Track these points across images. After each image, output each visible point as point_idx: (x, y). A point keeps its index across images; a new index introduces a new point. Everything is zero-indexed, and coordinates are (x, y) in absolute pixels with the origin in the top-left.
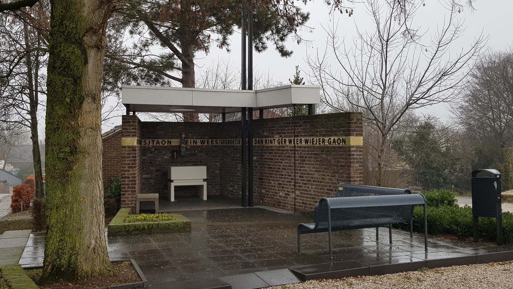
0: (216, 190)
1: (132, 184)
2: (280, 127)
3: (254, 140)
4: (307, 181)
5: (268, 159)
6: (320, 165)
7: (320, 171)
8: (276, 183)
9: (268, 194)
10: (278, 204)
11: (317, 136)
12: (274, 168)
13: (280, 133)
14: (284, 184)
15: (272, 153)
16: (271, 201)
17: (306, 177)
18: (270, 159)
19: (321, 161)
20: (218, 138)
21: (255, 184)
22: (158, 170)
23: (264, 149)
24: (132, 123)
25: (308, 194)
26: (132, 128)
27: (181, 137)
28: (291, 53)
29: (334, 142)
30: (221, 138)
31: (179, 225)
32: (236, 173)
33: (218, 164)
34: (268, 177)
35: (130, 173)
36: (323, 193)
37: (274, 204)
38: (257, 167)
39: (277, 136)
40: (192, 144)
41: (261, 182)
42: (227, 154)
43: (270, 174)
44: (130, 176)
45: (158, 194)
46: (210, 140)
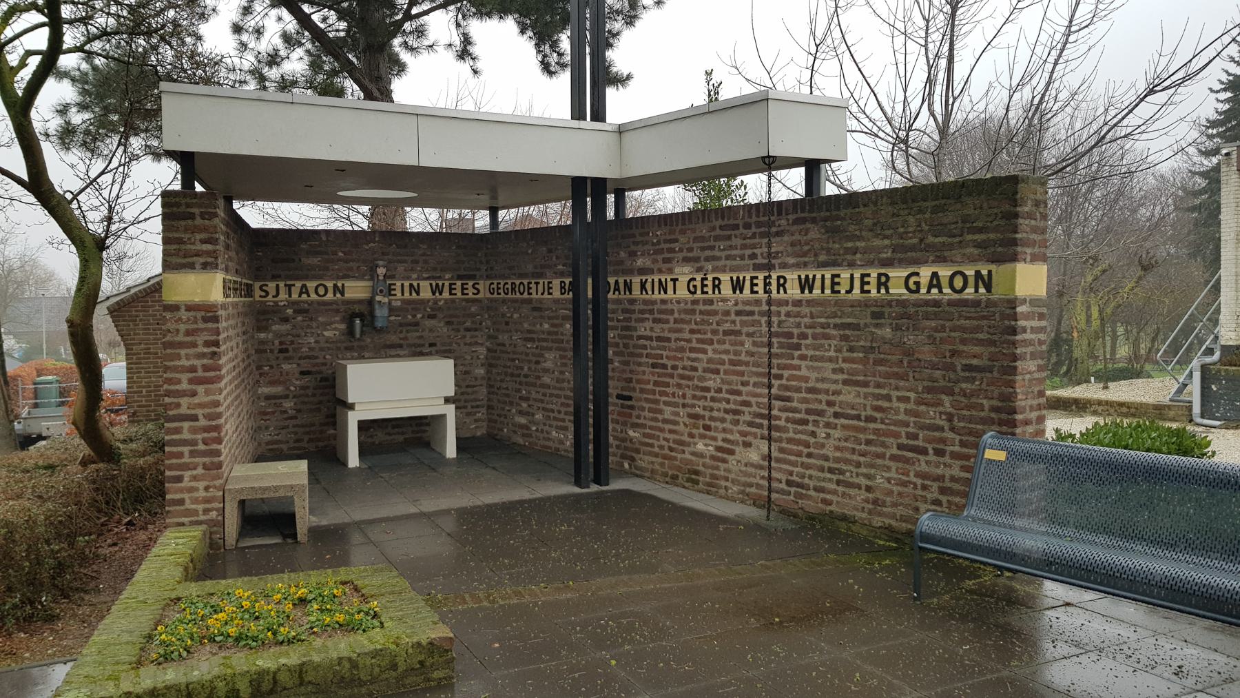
0: (476, 421)
1: (205, 442)
2: (696, 239)
4: (808, 412)
5: (650, 339)
6: (864, 361)
9: (652, 445)
10: (692, 478)
11: (852, 265)
12: (674, 367)
13: (697, 260)
14: (712, 419)
15: (667, 322)
16: (662, 465)
18: (659, 339)
19: (869, 350)
20: (481, 277)
22: (308, 373)
24: (199, 221)
25: (809, 455)
26: (198, 236)
27: (373, 275)
28: (629, 77)
29: (935, 280)
30: (488, 277)
31: (400, 661)
32: (539, 378)
33: (482, 351)
34: (654, 392)
35: (196, 400)
36: (882, 456)
39: (686, 269)
40: (407, 294)
41: (622, 406)
43: (656, 383)
45: (303, 465)
46: (459, 283)
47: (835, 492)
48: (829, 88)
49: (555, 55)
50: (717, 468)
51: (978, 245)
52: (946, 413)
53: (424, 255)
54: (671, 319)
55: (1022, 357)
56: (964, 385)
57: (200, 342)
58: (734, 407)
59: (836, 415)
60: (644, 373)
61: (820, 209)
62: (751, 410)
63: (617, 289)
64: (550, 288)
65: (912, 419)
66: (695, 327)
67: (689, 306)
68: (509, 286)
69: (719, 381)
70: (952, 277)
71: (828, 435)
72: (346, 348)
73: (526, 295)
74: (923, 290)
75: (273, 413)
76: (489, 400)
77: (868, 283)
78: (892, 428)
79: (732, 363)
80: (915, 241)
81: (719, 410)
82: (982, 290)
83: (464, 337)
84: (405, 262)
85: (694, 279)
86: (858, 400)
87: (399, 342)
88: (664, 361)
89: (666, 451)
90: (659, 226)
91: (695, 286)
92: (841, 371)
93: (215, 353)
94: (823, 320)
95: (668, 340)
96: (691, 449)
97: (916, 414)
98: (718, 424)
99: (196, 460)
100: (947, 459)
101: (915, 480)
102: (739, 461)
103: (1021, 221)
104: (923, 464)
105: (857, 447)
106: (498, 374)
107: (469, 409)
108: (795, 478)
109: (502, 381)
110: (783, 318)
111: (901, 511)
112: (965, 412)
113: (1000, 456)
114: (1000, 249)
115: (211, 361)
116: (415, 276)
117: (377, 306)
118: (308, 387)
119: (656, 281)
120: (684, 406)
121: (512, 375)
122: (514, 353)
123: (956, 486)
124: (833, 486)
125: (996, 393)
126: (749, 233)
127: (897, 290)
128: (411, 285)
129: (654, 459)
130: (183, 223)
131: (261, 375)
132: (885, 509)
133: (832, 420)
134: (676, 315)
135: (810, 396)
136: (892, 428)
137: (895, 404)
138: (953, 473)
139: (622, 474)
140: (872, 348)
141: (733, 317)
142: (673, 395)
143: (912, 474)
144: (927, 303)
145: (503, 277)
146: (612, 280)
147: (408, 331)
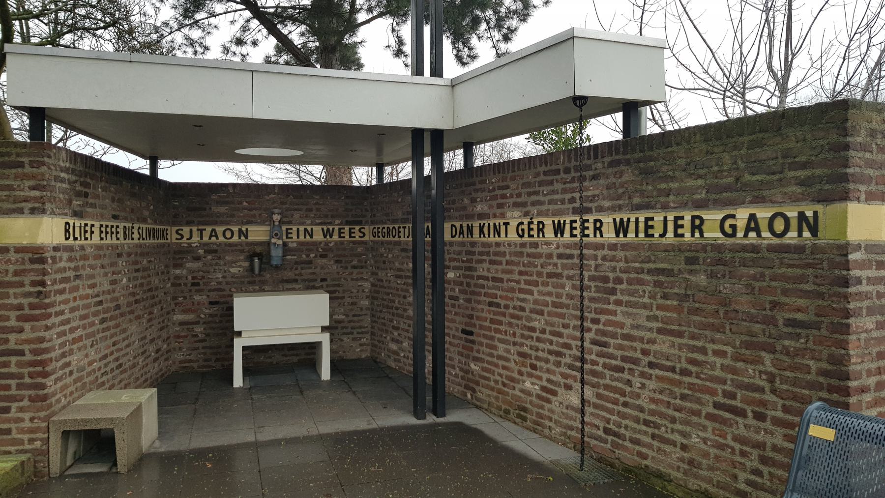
0: (361, 345)
1: (31, 376)
2: (524, 185)
3: (447, 226)
4: (624, 359)
5: (486, 278)
6: (678, 309)
7: (680, 335)
8: (513, 349)
9: (488, 379)
10: (519, 414)
11: (665, 207)
12: (507, 307)
13: (524, 205)
14: (537, 358)
15: (500, 263)
16: (497, 398)
17: (620, 347)
18: (494, 279)
20: (367, 223)
21: (450, 343)
24: (28, 169)
25: (625, 404)
29: (753, 223)
30: (373, 223)
33: (367, 285)
34: (489, 329)
35: (23, 336)
36: (697, 413)
37: (507, 412)
38: (456, 299)
39: (516, 214)
40: (302, 237)
41: (466, 340)
42: (384, 262)
43: (492, 321)
44: (26, 348)
46: (347, 228)
47: (650, 446)
48: (653, 34)
49: (466, 49)
50: (542, 407)
51: (801, 183)
52: (766, 373)
54: (504, 260)
55: (857, 313)
56: (787, 343)
57: (27, 282)
58: (556, 348)
59: (651, 365)
61: (634, 151)
62: (572, 352)
65: (730, 376)
66: (522, 269)
67: (518, 249)
68: (385, 230)
69: (543, 322)
70: (771, 220)
71: (643, 386)
72: (250, 283)
73: (396, 238)
74: (740, 234)
75: (186, 336)
76: (372, 327)
77: (682, 226)
78: (708, 384)
79: (555, 305)
80: (730, 180)
81: (543, 350)
82: (807, 234)
83: (352, 273)
84: (300, 210)
85: (522, 223)
86: (672, 351)
89: (500, 386)
90: (494, 174)
91: (523, 230)
92: (655, 318)
93: (41, 292)
94: (637, 265)
95: (501, 280)
96: (520, 386)
97: (734, 371)
98: (542, 364)
99: (23, 392)
100: (768, 425)
101: (732, 443)
102: (561, 403)
103: (852, 153)
104: (742, 427)
105: (672, 401)
106: (378, 305)
107: (355, 335)
108: (611, 426)
109: (381, 311)
110: (600, 262)
111: (718, 476)
112: (788, 373)
113: (829, 434)
114: (827, 187)
115: (37, 300)
116: (309, 222)
117: (272, 247)
118: (216, 315)
119: (492, 225)
120: (515, 344)
121: (388, 307)
122: (389, 288)
123: (778, 457)
124: (647, 440)
125: (825, 354)
126: (568, 177)
127: (712, 234)
128: (306, 230)
129: (491, 393)
130: (13, 171)
131: (176, 304)
132: (701, 472)
133: (647, 370)
134: (508, 257)
135: (625, 343)
136: (708, 384)
137: (711, 358)
138: (775, 441)
139: (463, 403)
140: (686, 295)
141: (555, 260)
142: (506, 332)
143: (729, 437)
144: (744, 248)
147: (302, 269)
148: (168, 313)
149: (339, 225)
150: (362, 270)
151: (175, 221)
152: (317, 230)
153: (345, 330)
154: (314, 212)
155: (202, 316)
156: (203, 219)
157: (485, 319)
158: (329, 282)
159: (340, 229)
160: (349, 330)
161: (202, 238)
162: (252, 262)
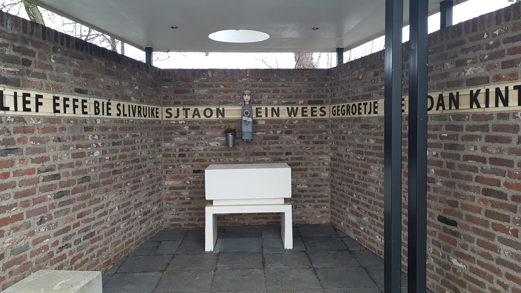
0: (322, 212)
5: (483, 160)
15: (508, 140)
18: (494, 161)
20: (327, 102)
23: (465, 124)
30: (333, 102)
32: (366, 186)
33: (327, 159)
40: (270, 116)
42: (344, 138)
46: (309, 107)
53: (283, 86)
60: (473, 199)
63: (440, 104)
64: (375, 107)
72: (226, 155)
76: (332, 197)
83: (314, 148)
87: (263, 151)
88: (502, 189)
95: (509, 163)
106: (337, 178)
107: (317, 203)
116: (275, 102)
117: (243, 124)
121: (347, 180)
122: (349, 162)
128: (273, 109)
131: (167, 172)
145: (342, 101)
146: (435, 96)
147: (270, 143)
148: (159, 179)
149: (301, 104)
150: (323, 145)
151: (165, 102)
152: (283, 109)
153: (307, 199)
154: (280, 93)
155: (188, 182)
156: (187, 100)
157: (479, 210)
158: (293, 155)
159: (303, 108)
160: (311, 198)
161: (187, 117)
162: (227, 136)
